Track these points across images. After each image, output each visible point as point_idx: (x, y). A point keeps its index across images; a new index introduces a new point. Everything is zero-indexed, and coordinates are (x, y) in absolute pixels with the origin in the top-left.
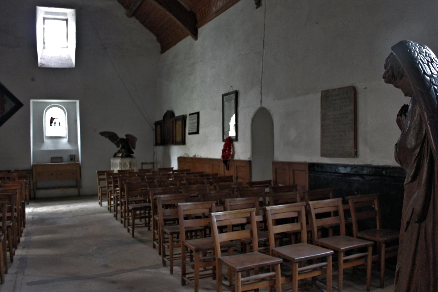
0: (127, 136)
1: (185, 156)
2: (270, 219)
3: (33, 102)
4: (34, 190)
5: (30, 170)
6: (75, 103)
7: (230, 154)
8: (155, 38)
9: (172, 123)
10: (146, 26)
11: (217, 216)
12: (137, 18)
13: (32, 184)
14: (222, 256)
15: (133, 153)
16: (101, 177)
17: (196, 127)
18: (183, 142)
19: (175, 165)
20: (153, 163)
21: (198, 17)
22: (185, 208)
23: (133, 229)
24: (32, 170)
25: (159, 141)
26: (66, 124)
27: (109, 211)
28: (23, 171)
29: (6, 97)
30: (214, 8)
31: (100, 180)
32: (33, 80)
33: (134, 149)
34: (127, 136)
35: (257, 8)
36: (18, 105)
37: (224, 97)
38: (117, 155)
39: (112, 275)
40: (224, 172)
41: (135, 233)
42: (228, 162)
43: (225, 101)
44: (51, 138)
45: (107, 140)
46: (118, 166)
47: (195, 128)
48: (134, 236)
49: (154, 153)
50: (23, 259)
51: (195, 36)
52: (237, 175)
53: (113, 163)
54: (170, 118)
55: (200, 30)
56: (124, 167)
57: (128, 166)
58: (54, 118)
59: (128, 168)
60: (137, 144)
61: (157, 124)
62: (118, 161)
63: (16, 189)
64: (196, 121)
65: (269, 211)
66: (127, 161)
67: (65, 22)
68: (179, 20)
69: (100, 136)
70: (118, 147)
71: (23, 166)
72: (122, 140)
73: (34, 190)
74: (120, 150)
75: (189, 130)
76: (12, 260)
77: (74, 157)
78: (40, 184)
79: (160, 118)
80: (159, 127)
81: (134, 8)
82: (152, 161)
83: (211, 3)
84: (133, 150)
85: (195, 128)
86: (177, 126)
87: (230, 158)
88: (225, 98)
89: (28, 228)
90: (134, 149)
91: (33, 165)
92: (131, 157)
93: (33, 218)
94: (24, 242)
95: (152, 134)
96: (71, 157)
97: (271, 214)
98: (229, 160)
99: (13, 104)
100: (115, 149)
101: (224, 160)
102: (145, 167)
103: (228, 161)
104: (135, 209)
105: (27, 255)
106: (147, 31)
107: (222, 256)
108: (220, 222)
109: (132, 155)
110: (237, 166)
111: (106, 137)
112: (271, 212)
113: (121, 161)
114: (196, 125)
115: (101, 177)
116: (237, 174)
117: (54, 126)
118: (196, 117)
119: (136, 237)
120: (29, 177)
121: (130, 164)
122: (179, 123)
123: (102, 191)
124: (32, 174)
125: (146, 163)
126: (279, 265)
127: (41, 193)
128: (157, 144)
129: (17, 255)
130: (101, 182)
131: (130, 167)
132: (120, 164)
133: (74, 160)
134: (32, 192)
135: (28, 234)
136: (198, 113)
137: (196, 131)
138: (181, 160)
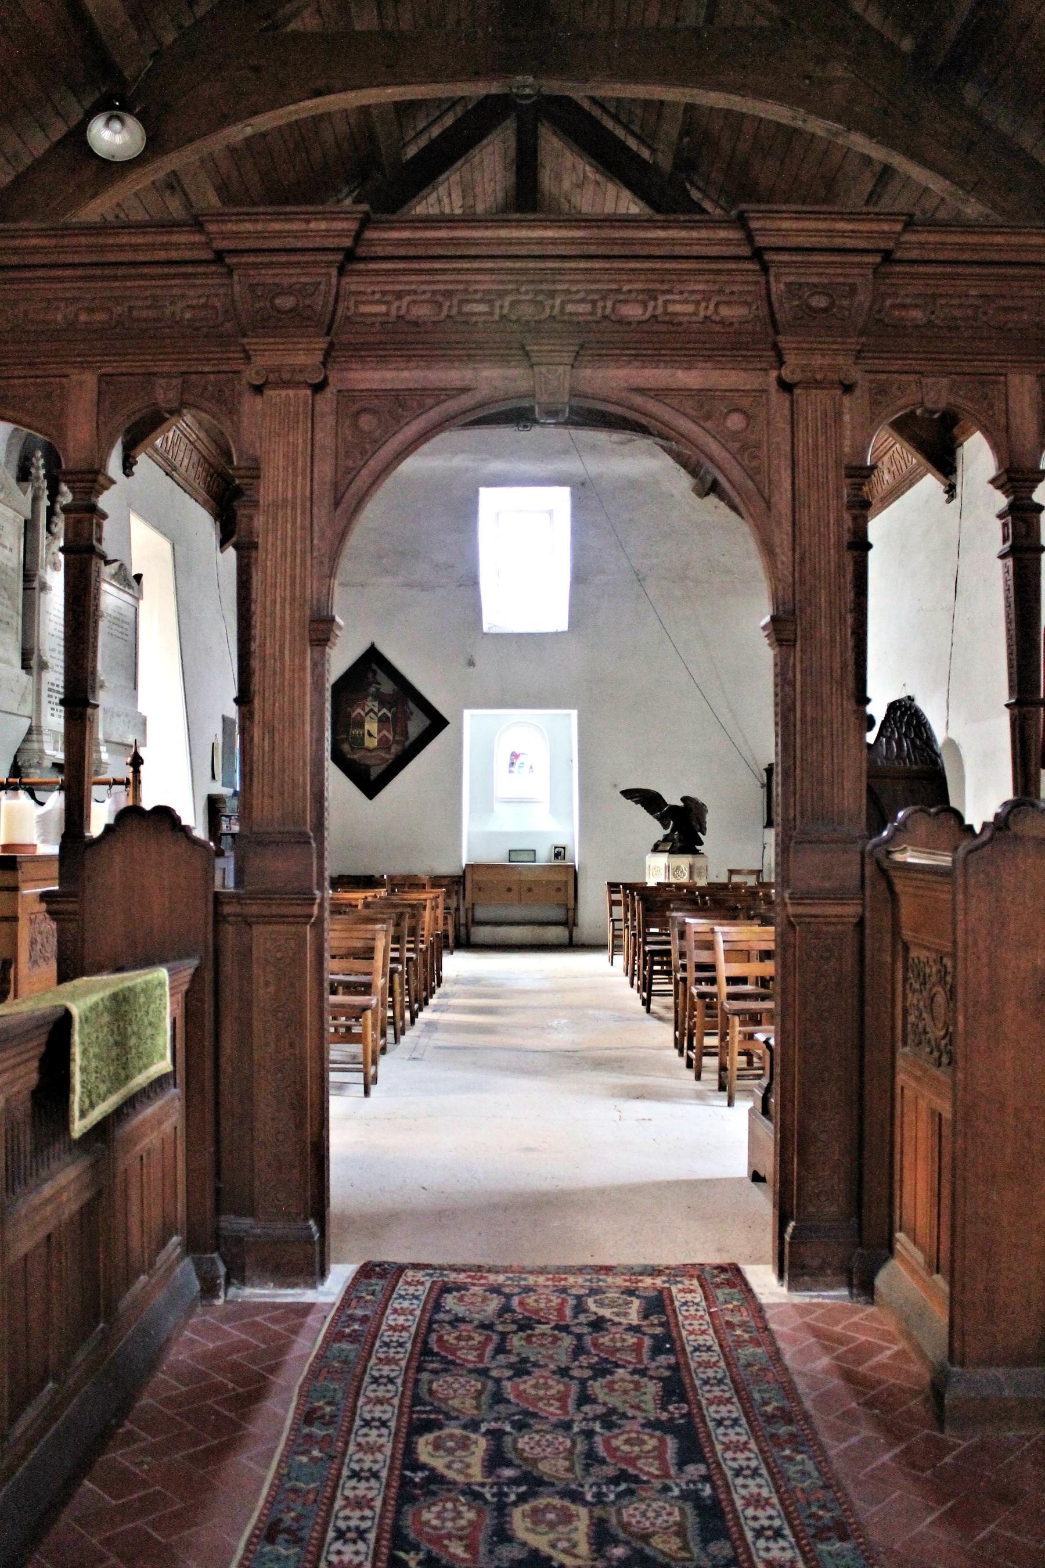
0: (684, 799)
6: (569, 715)
11: (723, 933)
13: (462, 912)
15: (701, 843)
16: (616, 897)
22: (699, 929)
24: (463, 876)
26: (571, 768)
28: (445, 877)
31: (613, 903)
32: (471, 663)
34: (684, 799)
35: (948, 501)
36: (437, 723)
44: (509, 801)
45: (639, 811)
59: (685, 879)
60: (711, 820)
62: (661, 860)
66: (684, 861)
67: (547, 516)
70: (665, 827)
71: (446, 868)
72: (674, 808)
76: (413, 1022)
78: (481, 914)
92: (696, 852)
100: (657, 831)
102: (736, 879)
111: (637, 802)
115: (616, 897)
120: (457, 893)
121: (691, 867)
123: (614, 929)
127: (482, 933)
131: (691, 877)
134: (463, 929)
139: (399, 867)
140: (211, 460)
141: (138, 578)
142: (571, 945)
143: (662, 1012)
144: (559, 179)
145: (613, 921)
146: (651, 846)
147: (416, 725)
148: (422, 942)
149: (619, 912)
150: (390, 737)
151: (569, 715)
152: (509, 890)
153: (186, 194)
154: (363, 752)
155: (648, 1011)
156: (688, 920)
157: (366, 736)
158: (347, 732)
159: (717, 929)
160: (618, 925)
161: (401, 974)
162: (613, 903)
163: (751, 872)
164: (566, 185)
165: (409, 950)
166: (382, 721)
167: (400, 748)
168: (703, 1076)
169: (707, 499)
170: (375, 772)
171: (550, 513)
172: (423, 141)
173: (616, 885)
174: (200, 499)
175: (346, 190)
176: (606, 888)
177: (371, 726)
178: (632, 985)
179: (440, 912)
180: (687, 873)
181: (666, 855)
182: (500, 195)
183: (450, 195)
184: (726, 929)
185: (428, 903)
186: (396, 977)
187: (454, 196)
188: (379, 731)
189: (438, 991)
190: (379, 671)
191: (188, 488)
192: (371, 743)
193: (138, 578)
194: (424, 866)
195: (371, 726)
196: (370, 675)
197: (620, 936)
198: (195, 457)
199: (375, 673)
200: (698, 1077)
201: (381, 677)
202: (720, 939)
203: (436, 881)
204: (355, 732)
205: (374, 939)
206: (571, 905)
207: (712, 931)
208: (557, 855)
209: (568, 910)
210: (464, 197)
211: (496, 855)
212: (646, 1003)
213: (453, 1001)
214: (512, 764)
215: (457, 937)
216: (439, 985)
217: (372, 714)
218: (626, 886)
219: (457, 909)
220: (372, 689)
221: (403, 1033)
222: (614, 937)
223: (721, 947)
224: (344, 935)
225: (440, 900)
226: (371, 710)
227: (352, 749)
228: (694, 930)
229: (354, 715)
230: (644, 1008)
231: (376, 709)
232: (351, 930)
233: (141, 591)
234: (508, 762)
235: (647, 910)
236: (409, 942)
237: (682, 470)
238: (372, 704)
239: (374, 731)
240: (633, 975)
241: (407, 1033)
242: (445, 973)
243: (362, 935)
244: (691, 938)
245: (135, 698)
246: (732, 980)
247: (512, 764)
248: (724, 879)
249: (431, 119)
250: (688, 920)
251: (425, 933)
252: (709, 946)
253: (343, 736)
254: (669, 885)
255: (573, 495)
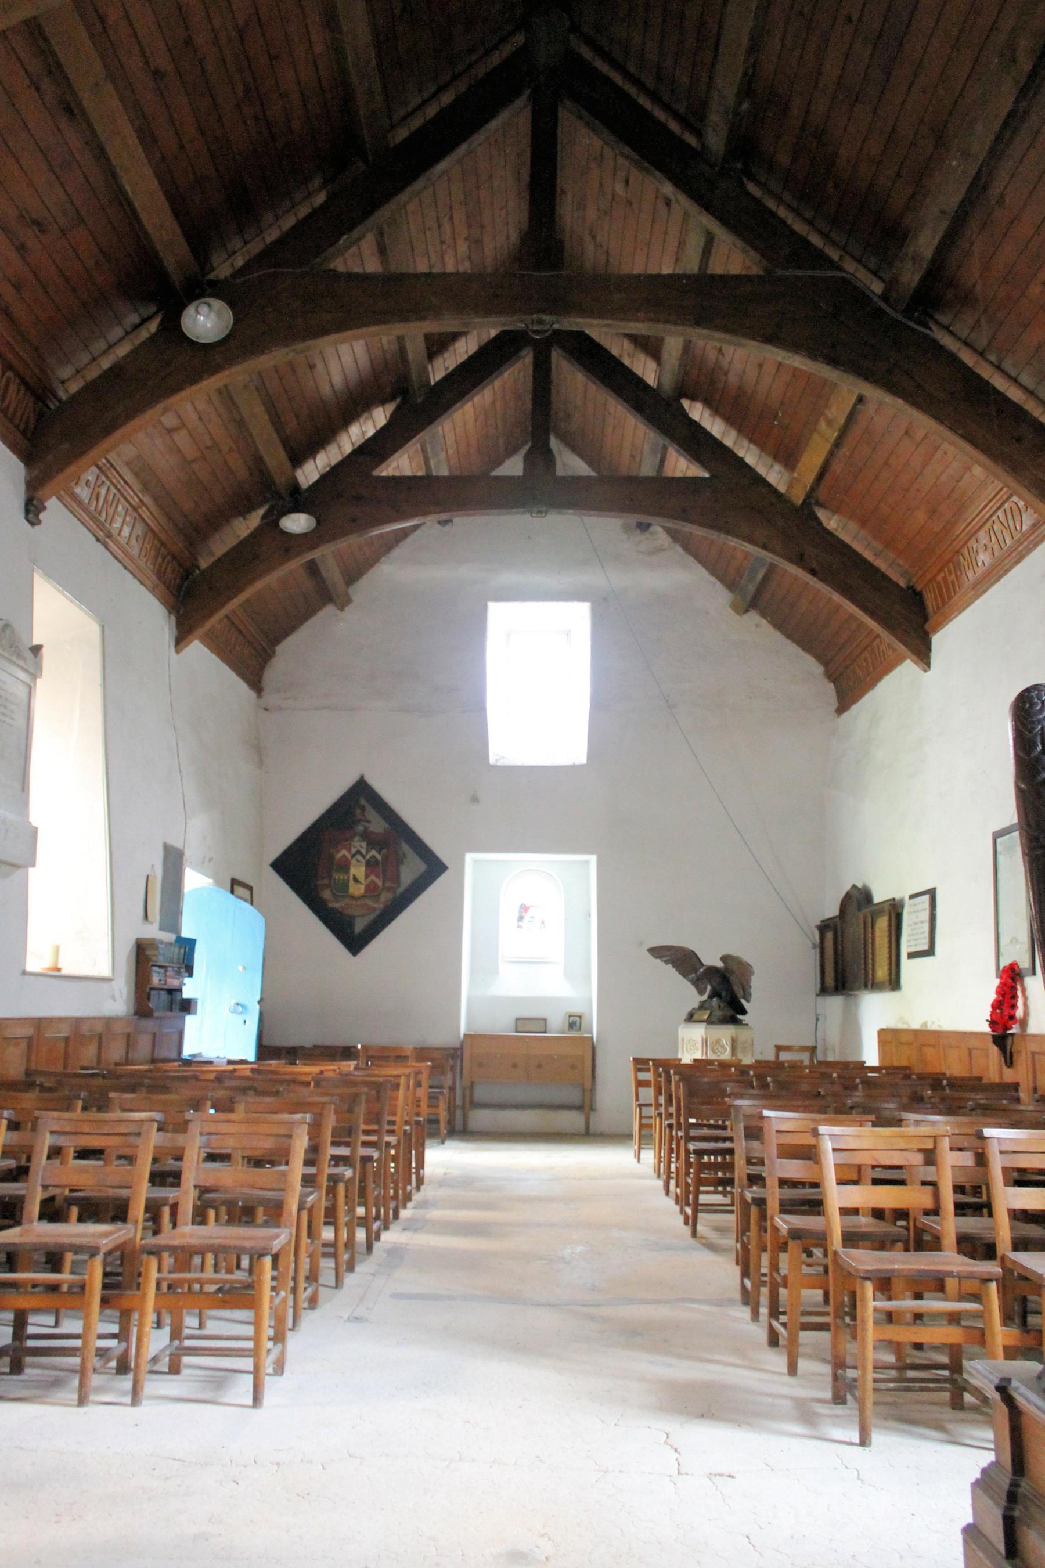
0: (725, 959)
1: (900, 1026)
2: (997, 1165)
3: (475, 861)
4: (463, 1107)
5: (455, 1049)
6: (587, 862)
7: (1012, 1017)
8: (819, 669)
9: (865, 923)
10: (790, 634)
12: (764, 615)
13: (458, 1092)
14: (844, 1246)
15: (744, 1012)
16: (643, 1076)
17: (927, 935)
18: (894, 983)
19: (871, 1056)
20: (813, 1049)
21: (930, 604)
22: (783, 1128)
23: (696, 1212)
24: (462, 1048)
25: (830, 981)
26: (589, 922)
27: (655, 1175)
29: (405, 848)
30: (970, 574)
31: (640, 1084)
32: (475, 800)
33: (748, 1001)
34: (725, 959)
37: (998, 840)
38: (696, 1017)
39: (598, 1306)
40: (1001, 1073)
41: (699, 1228)
42: (1009, 1041)
43: (1000, 853)
46: (697, 1050)
47: (925, 938)
48: (698, 1235)
49: (817, 1019)
50: (396, 1252)
51: (923, 654)
52: (1035, 1082)
53: (683, 1040)
54: (859, 910)
55: (936, 640)
56: (713, 1051)
57: (726, 1050)
58: (528, 905)
59: (726, 1055)
60: (757, 984)
61: (824, 927)
63: (399, 1076)
64: (926, 915)
65: (995, 1142)
66: (725, 1033)
68: (872, 614)
69: (649, 957)
70: (701, 992)
71: (439, 1038)
72: (712, 971)
73: (463, 1107)
74: (705, 1002)
75: (910, 944)
76: (369, 1248)
77: (578, 1019)
79: (832, 910)
80: (829, 935)
81: (751, 588)
82: (810, 1043)
83: (961, 558)
84: (743, 1001)
85: (925, 938)
86: (878, 933)
87: (1015, 1030)
88: (1000, 844)
89: (427, 1192)
90: (748, 1001)
91: (465, 1035)
92: (734, 1021)
93: (445, 1174)
94: (408, 1220)
95: (812, 958)
96: (572, 1019)
97: (1001, 1152)
98: (1012, 1035)
99: (422, 867)
100: (691, 996)
101: (995, 1034)
102: (784, 1056)
103: (1010, 1038)
104: (699, 1153)
105: (407, 1244)
106: (792, 648)
107: (844, 1246)
108: (844, 1154)
109: (740, 1017)
110: (1033, 1054)
111: (667, 962)
112: (1000, 1144)
113: (706, 1033)
114: (926, 927)
115: (643, 1076)
116: (1035, 1077)
117: (519, 927)
118: (927, 905)
119: (702, 1237)
120: (453, 1068)
121: (734, 1042)
122: (882, 924)
123: (641, 1117)
124: (462, 1060)
125: (787, 1048)
126: (993, 1286)
127: (480, 1118)
128: (824, 991)
129: (386, 1242)
130: (642, 1091)
132: (705, 1042)
133: (580, 1029)
134: (459, 1113)
135: (424, 1204)
136: (932, 893)
137: (925, 947)
138: (888, 1037)
139: (383, 1038)
140: (163, 536)
141: (36, 650)
142: (588, 1135)
143: (713, 1237)
144: (582, 206)
145: (640, 1106)
146: (685, 1015)
147: (411, 869)
148: (391, 1132)
149: (648, 1094)
150: (380, 884)
151: (587, 862)
152: (515, 1066)
153: (90, 126)
154: (347, 901)
155: (694, 1233)
156: (766, 1113)
157: (352, 882)
158: (330, 877)
159: (823, 1129)
160: (646, 1111)
161: (349, 1182)
162: (640, 1084)
163: (803, 1049)
164: (591, 213)
165: (365, 1144)
166: (371, 865)
167: (390, 896)
168: (803, 1364)
169: (746, 617)
170: (359, 926)
171: (568, 634)
172: (417, 122)
173: (645, 1061)
174: (147, 582)
175: (317, 181)
176: (631, 1066)
177: (358, 870)
178: (667, 1192)
179: (422, 1093)
180: (728, 1048)
181: (704, 1025)
182: (514, 237)
183: (451, 218)
184: (837, 1130)
185: (402, 1081)
186: (341, 1187)
187: (456, 217)
188: (367, 876)
189: (417, 1197)
190: (367, 806)
191: (131, 566)
192: (357, 890)
193: (36, 650)
194: (409, 1038)
195: (358, 870)
196: (358, 812)
197: (650, 1126)
198: (139, 530)
199: (363, 809)
200: (792, 1369)
201: (371, 814)
202: (828, 1145)
203: (422, 1053)
204: (336, 876)
205: (290, 1136)
206: (588, 1084)
207: (815, 1133)
208: (572, 1025)
209: (584, 1090)
210: (470, 226)
211: (501, 1024)
212: (691, 1222)
213: (435, 1214)
214: (521, 918)
215: (450, 1122)
216: (418, 1188)
217: (359, 857)
218: (657, 1063)
219: (452, 1089)
220: (360, 828)
221: (351, 1268)
222: (642, 1126)
223: (830, 1160)
224: (243, 1128)
225: (424, 1077)
226: (359, 852)
227: (334, 895)
228: (776, 1128)
229: (339, 856)
230: (687, 1230)
231: (364, 851)
232: (256, 1122)
233: (39, 667)
234: (517, 915)
235: (691, 1094)
236: (367, 1132)
237: (718, 584)
238: (359, 844)
239: (361, 876)
240: (669, 1178)
241: (358, 1268)
242: (428, 1170)
243: (275, 1130)
244: (773, 1141)
245: (26, 803)
246: (845, 1212)
247: (521, 918)
248: (770, 1056)
249: (426, 95)
250: (766, 1113)
251: (397, 1119)
252: (809, 1153)
253: (326, 881)
254: (709, 1062)
255: (594, 611)
